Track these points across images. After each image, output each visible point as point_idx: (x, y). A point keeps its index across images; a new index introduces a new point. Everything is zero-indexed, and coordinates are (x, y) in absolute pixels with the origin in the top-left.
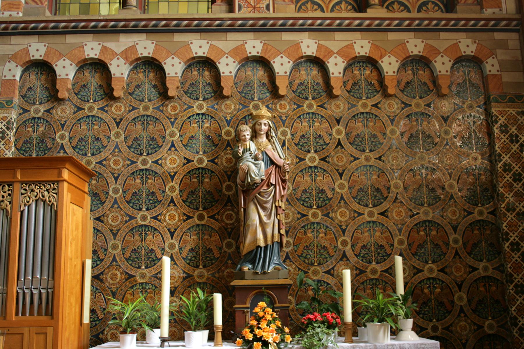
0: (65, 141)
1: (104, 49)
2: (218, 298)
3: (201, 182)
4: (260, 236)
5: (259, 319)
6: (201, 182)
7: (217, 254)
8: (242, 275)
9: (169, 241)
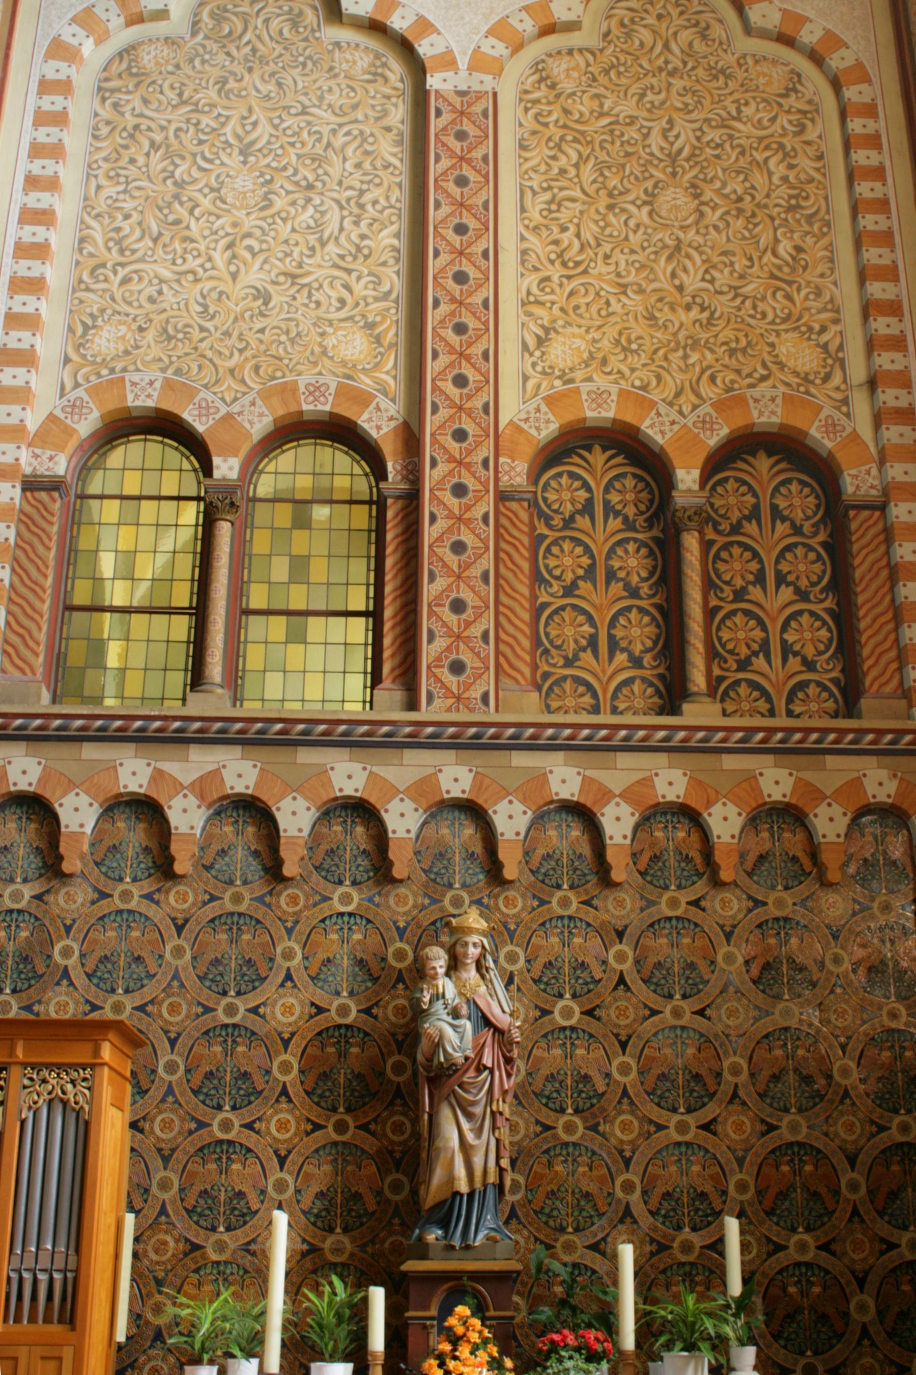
0: (72, 962)
1: (158, 776)
2: (378, 1296)
3: (342, 1055)
4: (460, 1171)
5: (455, 1340)
6: (342, 1055)
7: (371, 1204)
8: (422, 1251)
9: (276, 1175)
